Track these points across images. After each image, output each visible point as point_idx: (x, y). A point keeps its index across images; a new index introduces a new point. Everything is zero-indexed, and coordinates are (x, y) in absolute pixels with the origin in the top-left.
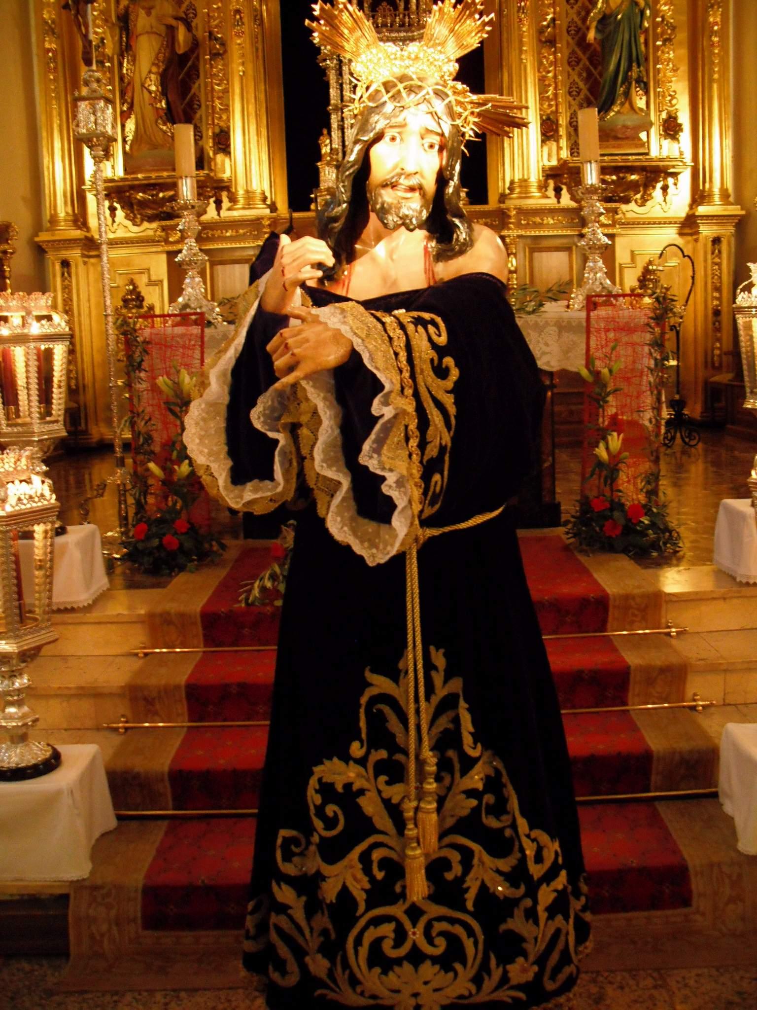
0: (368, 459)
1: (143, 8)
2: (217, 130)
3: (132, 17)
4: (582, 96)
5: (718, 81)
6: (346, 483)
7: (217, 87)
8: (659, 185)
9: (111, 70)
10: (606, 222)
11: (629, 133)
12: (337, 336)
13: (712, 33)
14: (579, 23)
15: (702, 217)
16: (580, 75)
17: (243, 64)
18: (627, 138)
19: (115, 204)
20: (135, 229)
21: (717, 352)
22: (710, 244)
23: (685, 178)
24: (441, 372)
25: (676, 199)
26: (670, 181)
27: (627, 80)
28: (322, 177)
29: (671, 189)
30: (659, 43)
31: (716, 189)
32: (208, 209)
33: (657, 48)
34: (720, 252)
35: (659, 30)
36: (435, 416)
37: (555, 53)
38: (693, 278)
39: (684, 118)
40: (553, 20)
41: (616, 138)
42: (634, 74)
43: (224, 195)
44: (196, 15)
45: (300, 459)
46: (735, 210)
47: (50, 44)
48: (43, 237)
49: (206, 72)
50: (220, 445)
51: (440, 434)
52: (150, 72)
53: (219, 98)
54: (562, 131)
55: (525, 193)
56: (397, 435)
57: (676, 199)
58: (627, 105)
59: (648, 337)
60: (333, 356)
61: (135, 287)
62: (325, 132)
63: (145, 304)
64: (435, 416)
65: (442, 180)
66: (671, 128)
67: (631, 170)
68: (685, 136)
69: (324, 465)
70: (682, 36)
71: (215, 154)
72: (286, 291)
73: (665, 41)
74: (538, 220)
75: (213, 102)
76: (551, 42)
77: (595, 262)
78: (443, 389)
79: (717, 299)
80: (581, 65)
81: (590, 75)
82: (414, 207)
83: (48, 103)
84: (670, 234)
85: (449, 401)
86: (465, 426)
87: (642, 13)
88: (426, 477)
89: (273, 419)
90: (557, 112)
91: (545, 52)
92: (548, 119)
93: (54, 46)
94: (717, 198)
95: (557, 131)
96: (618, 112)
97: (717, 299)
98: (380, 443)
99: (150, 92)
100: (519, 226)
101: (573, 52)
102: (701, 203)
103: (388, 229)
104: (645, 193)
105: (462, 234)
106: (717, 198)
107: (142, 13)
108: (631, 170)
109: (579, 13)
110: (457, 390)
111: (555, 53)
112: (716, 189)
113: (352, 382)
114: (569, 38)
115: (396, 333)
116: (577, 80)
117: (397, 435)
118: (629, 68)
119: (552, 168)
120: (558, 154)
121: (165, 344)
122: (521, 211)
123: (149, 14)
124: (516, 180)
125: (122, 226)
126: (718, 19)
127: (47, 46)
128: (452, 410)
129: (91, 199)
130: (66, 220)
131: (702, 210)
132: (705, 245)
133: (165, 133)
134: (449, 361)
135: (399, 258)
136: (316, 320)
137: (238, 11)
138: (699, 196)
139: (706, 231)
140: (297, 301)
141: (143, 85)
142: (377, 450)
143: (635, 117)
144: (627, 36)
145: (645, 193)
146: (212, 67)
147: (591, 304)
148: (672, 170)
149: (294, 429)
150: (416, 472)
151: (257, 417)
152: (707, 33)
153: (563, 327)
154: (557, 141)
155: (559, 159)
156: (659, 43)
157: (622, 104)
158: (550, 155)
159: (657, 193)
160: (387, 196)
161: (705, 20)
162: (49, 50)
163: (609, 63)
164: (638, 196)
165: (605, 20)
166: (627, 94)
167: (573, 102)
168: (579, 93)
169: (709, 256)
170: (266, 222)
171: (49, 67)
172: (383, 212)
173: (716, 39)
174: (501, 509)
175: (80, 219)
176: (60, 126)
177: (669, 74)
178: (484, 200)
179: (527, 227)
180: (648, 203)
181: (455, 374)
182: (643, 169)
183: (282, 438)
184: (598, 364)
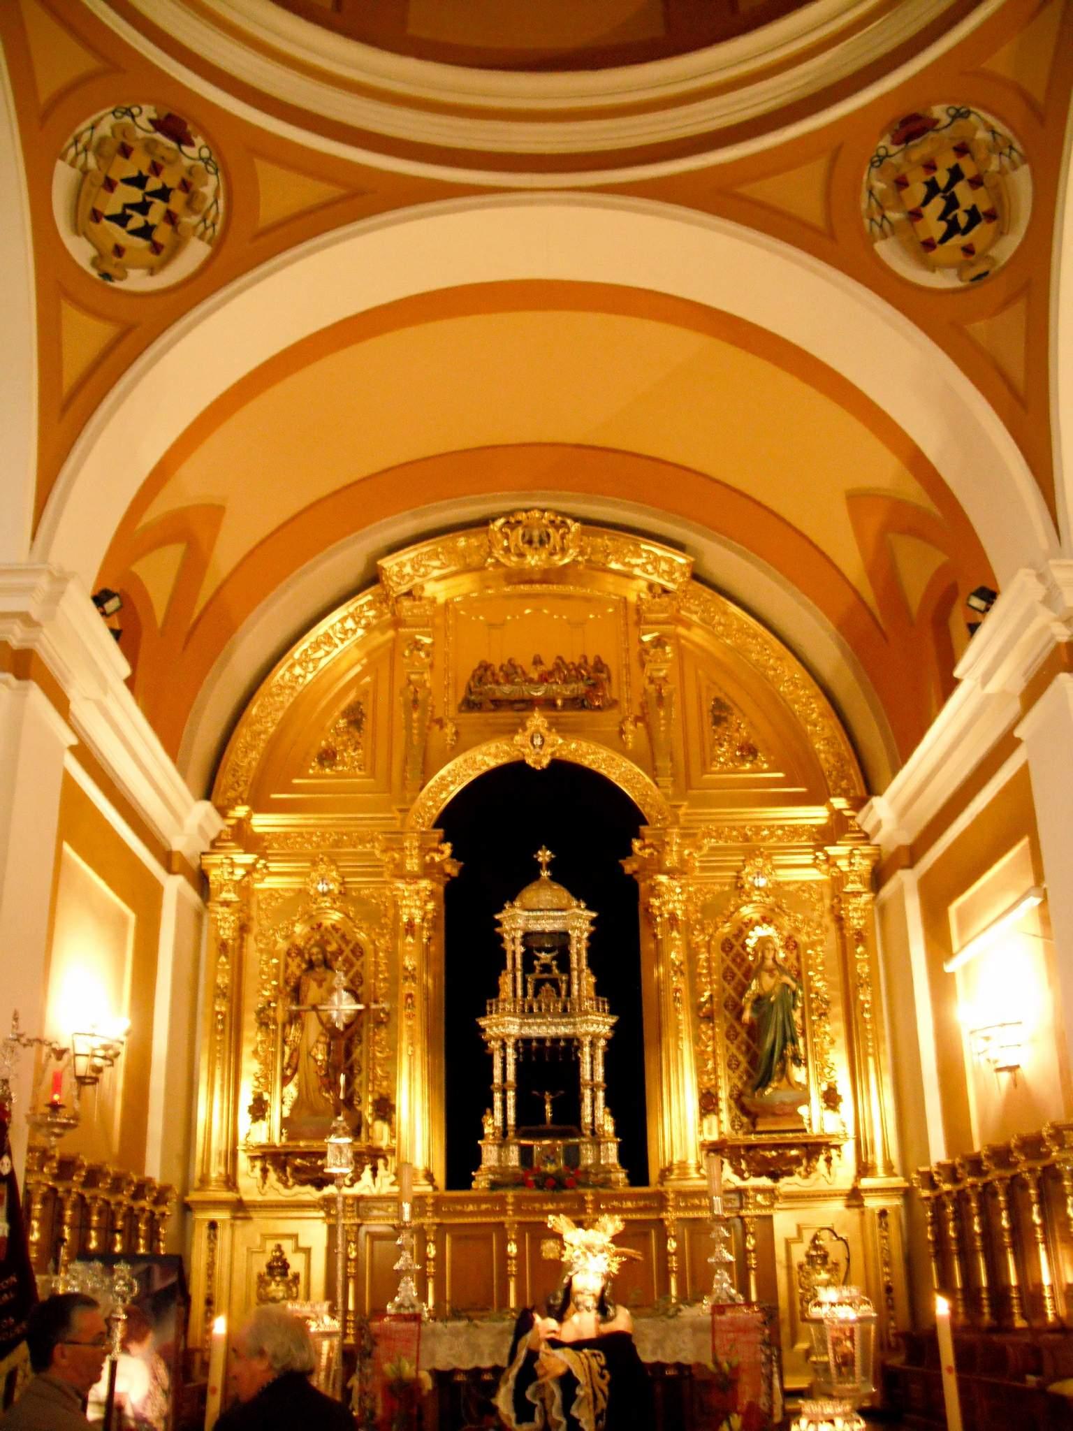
0: (574, 1412)
1: (315, 980)
2: (377, 1097)
3: (304, 988)
4: (742, 1068)
5: (874, 1055)
6: (565, 1422)
7: (378, 1055)
8: (822, 1158)
9: (275, 1031)
10: (763, 1203)
11: (788, 1109)
12: (563, 1363)
13: (864, 1010)
14: (737, 998)
15: (866, 1190)
16: (739, 1048)
17: (412, 1044)
18: (785, 1114)
19: (269, 1167)
20: (286, 1192)
21: (891, 1331)
22: (876, 1217)
23: (849, 1148)
24: (602, 1376)
25: (843, 1171)
26: (834, 1152)
27: (782, 1057)
28: (485, 1155)
29: (835, 1161)
30: (814, 1018)
31: (879, 1161)
32: (363, 1176)
33: (813, 1022)
34: (887, 1225)
35: (814, 1005)
36: (600, 1396)
37: (713, 1028)
38: (848, 1260)
39: (844, 1089)
40: (711, 996)
41: (774, 1114)
42: (789, 1052)
43: (381, 1162)
44: (362, 983)
45: (546, 1413)
46: (898, 1181)
47: (221, 1007)
48: (193, 1196)
49: (368, 1039)
50: (511, 1407)
51: (602, 1404)
52: (318, 1041)
53: (380, 1065)
54: (723, 1105)
55: (684, 1175)
56: (586, 1402)
57: (843, 1171)
58: (785, 1080)
59: (760, 1337)
60: (561, 1370)
61: (282, 1253)
62: (488, 1111)
63: (290, 1272)
64: (600, 1396)
65: (603, 1290)
66: (831, 1098)
67: (791, 1146)
68: (846, 1105)
69: (556, 1414)
70: (837, 1010)
71: (374, 1120)
72: (539, 1341)
73: (821, 1015)
74: (696, 1202)
75: (374, 1068)
76: (709, 1018)
77: (721, 1275)
78: (603, 1384)
79: (887, 1274)
80: (739, 1039)
81: (749, 1048)
82: (591, 1302)
83: (212, 1064)
84: (838, 1205)
85: (606, 1389)
86: (611, 1401)
87: (794, 993)
88: (597, 1422)
89: (534, 1395)
90: (716, 1086)
91: (703, 1027)
92: (709, 1093)
93: (223, 1009)
94: (880, 1170)
95: (717, 1104)
96: (776, 1089)
97: (887, 1274)
98: (580, 1404)
99: (316, 1061)
100: (677, 1208)
101: (732, 1027)
102: (864, 1176)
103: (578, 1310)
104: (809, 1165)
105: (611, 1312)
106: (880, 1170)
107: (314, 985)
108: (791, 1146)
109: (735, 989)
110: (609, 1385)
111: (713, 1028)
112: (879, 1161)
113: (568, 1381)
114: (727, 1013)
115: (585, 1361)
116: (737, 1054)
117: (586, 1402)
118: (784, 1047)
119: (713, 1144)
120: (719, 1127)
121: (387, 1335)
122: (681, 1194)
123: (320, 985)
124: (675, 1162)
125: (276, 1190)
126: (869, 998)
127: (217, 1008)
128: (607, 1393)
129: (243, 1162)
130: (217, 1181)
131: (866, 1183)
132: (872, 1218)
133: (327, 1100)
134: (606, 1372)
135: (583, 1323)
136: (554, 1356)
137: (410, 996)
138: (864, 1169)
139: (873, 1203)
140: (543, 1347)
141: (309, 1053)
142: (578, 1408)
143: (792, 1093)
144: (780, 1016)
145: (809, 1165)
146: (375, 1034)
147: (718, 1309)
148: (834, 1143)
149: (543, 1400)
150: (593, 1418)
151: (529, 1394)
152: (859, 1010)
153: (696, 1328)
154: (717, 1114)
155: (721, 1133)
156: (814, 1018)
157: (780, 1081)
158: (710, 1128)
159: (821, 1164)
160: (579, 1298)
161: (856, 998)
162: (218, 1013)
163: (764, 1043)
164: (802, 1169)
165: (759, 1000)
166: (784, 1072)
167: (733, 1075)
168: (738, 1066)
169: (877, 1230)
170: (430, 1201)
171: (216, 1029)
172: (577, 1305)
173: (867, 1016)
174: (141, 525)
175: (230, 1182)
176: (222, 1086)
177: (826, 1046)
178: (645, 1182)
179: (686, 1208)
180: (813, 1176)
181: (608, 1377)
182: (805, 1145)
183: (537, 1402)
184: (721, 1358)
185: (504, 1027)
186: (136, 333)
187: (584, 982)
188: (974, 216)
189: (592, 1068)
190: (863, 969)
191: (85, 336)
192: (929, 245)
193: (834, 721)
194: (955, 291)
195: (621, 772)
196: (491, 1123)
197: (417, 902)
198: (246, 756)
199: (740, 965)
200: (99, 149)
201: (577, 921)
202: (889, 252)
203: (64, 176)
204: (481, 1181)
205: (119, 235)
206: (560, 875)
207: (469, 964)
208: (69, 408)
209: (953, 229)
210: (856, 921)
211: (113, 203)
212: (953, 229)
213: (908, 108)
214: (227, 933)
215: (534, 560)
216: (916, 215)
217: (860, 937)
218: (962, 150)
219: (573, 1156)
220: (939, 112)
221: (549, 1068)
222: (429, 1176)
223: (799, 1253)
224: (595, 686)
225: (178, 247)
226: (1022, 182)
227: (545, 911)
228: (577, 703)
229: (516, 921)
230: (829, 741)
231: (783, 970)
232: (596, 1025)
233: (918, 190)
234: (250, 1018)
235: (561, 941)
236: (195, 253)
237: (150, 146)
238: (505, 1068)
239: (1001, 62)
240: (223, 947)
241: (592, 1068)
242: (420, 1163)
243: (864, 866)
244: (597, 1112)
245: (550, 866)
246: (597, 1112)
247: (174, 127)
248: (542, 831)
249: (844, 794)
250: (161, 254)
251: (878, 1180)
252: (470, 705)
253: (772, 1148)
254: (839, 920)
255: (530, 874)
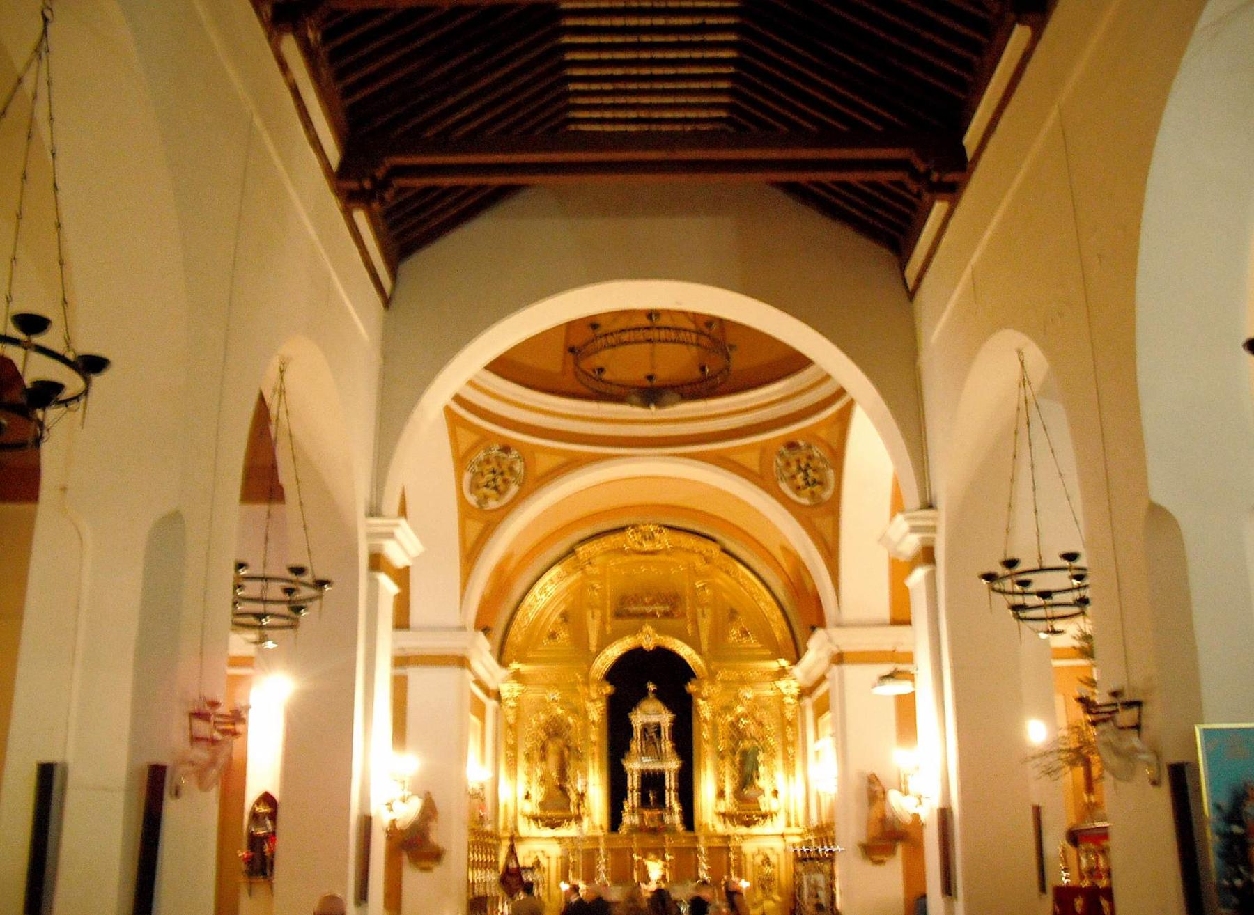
46: (799, 831)
185: (635, 766)
186: (491, 525)
187: (667, 745)
188: (815, 482)
189: (671, 782)
190: (790, 738)
191: (475, 527)
192: (799, 488)
193: (784, 623)
194: (808, 506)
195: (684, 651)
196: (627, 806)
197: (596, 711)
198: (517, 636)
199: (737, 734)
200: (480, 464)
201: (665, 719)
202: (784, 486)
203: (467, 476)
204: (623, 830)
205: (485, 490)
206: (659, 695)
207: (618, 738)
208: (470, 555)
209: (808, 484)
210: (789, 715)
211: (483, 481)
212: (808, 484)
213: (791, 439)
214: (511, 720)
215: (647, 546)
216: (793, 477)
217: (790, 723)
218: (810, 458)
219: (661, 818)
220: (801, 443)
221: (652, 781)
222: (602, 828)
223: (759, 859)
224: (674, 607)
225: (507, 489)
226: (831, 474)
227: (651, 714)
228: (666, 615)
229: (638, 719)
230: (782, 631)
231: (753, 738)
232: (672, 765)
233: (794, 468)
234: (521, 757)
235: (658, 727)
236: (514, 489)
237: (497, 457)
238: (633, 782)
239: (823, 434)
240: (510, 727)
241: (671, 782)
242: (597, 823)
243: (795, 691)
244: (671, 799)
245: (654, 692)
246: (671, 799)
247: (506, 449)
248: (653, 676)
249: (786, 658)
250: (501, 493)
251: (794, 830)
252: (618, 615)
253: (747, 812)
254: (783, 715)
255: (644, 694)
